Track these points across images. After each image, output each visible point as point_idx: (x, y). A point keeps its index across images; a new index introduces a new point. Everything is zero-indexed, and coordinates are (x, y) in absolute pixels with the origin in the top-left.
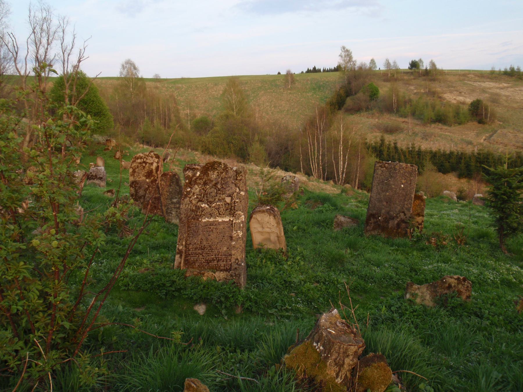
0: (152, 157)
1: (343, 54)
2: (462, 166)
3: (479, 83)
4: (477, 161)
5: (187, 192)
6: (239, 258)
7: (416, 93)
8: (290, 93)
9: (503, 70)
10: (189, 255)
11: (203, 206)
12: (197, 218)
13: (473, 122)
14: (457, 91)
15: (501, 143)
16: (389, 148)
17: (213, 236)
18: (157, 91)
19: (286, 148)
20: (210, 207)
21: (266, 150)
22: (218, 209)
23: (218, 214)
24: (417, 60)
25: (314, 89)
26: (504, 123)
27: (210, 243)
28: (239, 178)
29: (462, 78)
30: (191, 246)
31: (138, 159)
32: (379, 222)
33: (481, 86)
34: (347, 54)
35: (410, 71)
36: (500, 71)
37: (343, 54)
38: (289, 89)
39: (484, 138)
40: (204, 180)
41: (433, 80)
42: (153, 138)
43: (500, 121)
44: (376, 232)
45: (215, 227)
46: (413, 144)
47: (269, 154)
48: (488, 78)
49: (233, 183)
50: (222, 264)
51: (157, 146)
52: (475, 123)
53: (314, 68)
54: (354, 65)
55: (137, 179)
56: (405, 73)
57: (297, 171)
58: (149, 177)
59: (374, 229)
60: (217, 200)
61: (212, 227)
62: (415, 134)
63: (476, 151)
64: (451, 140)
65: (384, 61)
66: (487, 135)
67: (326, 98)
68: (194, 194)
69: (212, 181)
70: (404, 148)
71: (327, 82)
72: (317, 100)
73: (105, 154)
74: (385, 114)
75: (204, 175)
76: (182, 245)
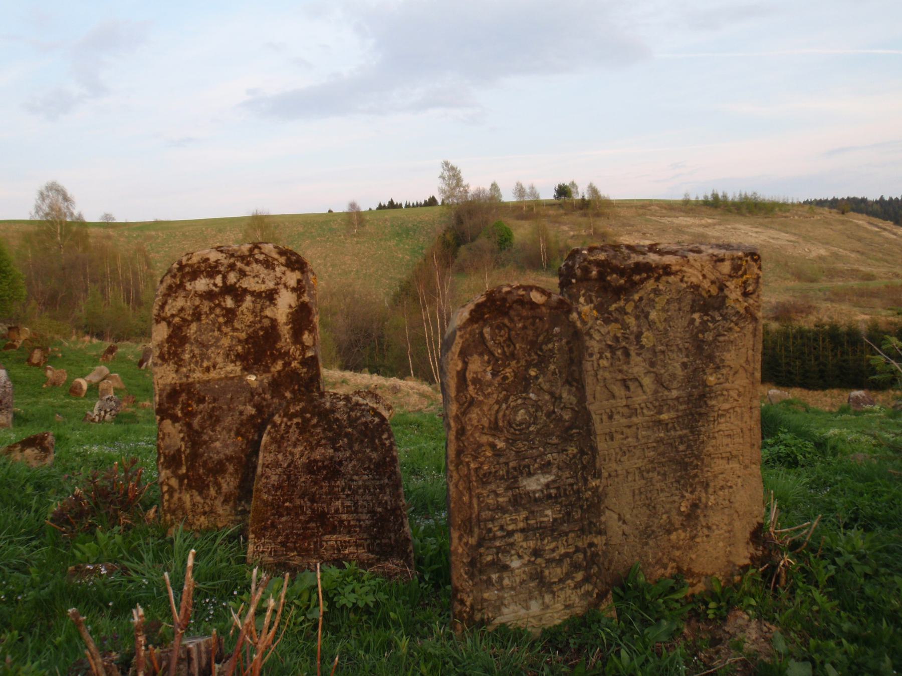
0: (268, 264)
1: (446, 174)
3: (669, 219)
7: (574, 236)
8: (357, 243)
9: (701, 198)
14: (638, 231)
18: (110, 243)
24: (567, 184)
25: (398, 235)
29: (641, 211)
31: (195, 274)
33: (672, 223)
34: (453, 175)
35: (557, 201)
36: (697, 201)
37: (446, 174)
38: (354, 236)
41: (598, 215)
42: (108, 325)
48: (681, 211)
51: (119, 339)
53: (391, 203)
54: (466, 192)
55: (197, 375)
56: (549, 205)
57: (406, 376)
58: (257, 361)
65: (513, 186)
67: (422, 248)
71: (420, 222)
72: (403, 257)
73: (7, 357)
74: (528, 272)
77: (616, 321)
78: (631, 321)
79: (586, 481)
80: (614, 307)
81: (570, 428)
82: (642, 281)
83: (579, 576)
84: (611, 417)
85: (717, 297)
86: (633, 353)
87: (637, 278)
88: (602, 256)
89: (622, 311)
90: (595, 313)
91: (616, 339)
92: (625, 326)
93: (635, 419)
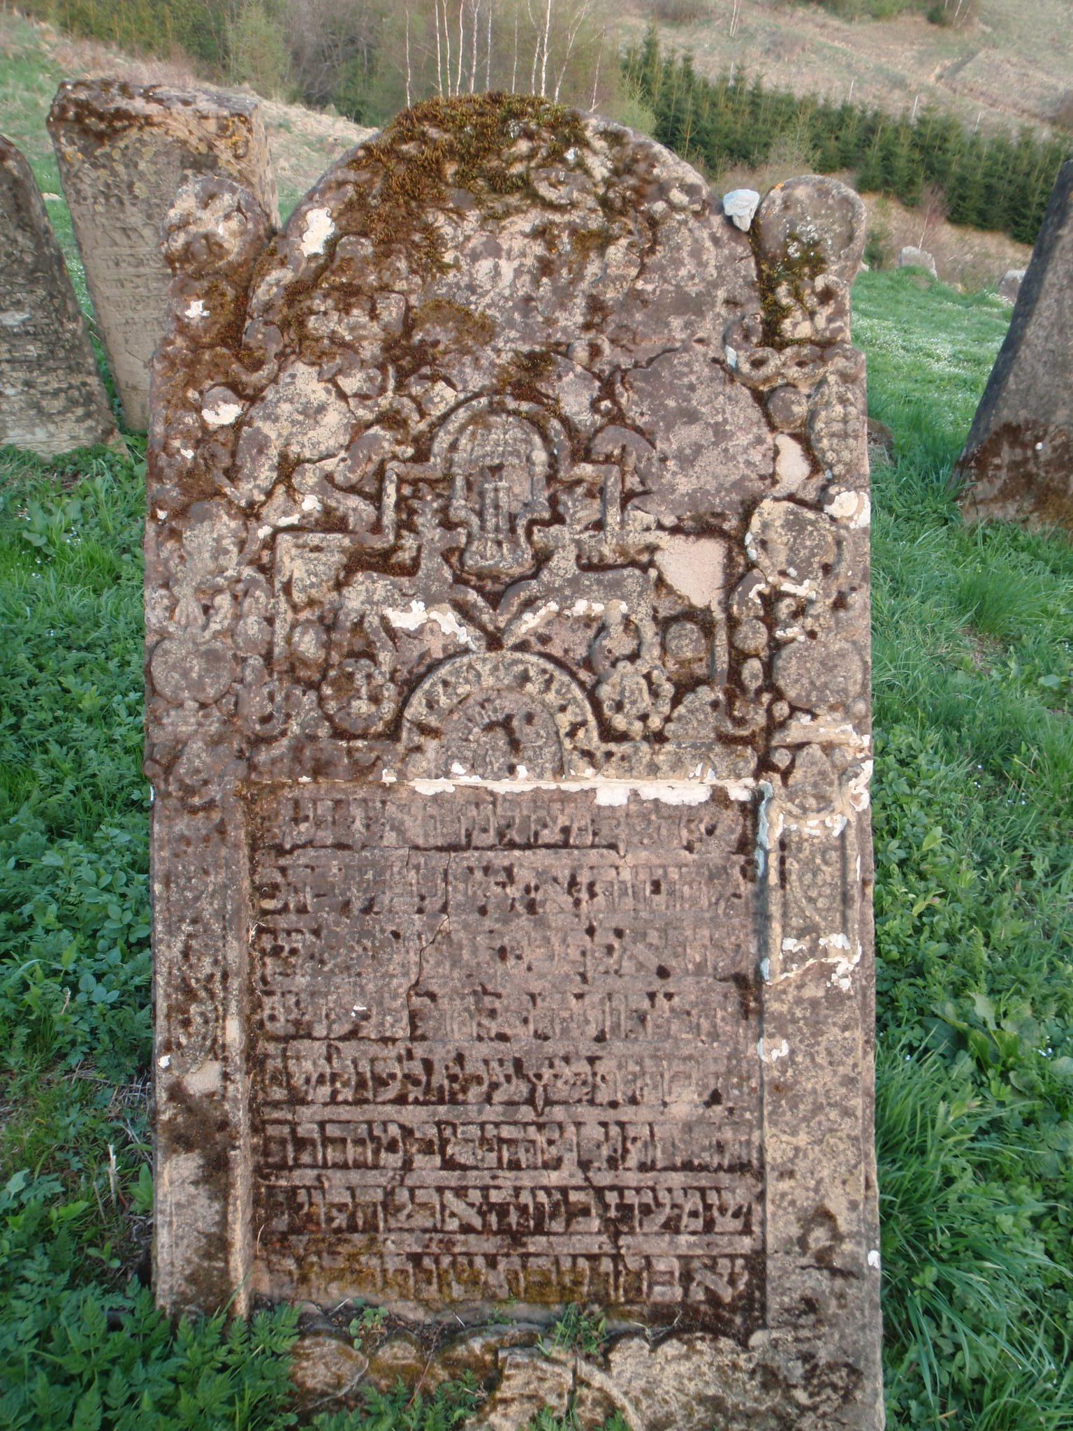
2: (874, 154)
4: (914, 145)
5: (203, 438)
6: (837, 1204)
10: (301, 1144)
11: (408, 618)
12: (359, 750)
13: (913, 14)
15: (982, 94)
16: (668, 75)
17: (545, 956)
19: (353, 41)
20: (494, 641)
21: (287, 41)
22: (588, 670)
23: (591, 738)
26: (995, 29)
27: (523, 1035)
28: (797, 327)
30: (308, 1062)
32: (1031, 467)
39: (938, 70)
40: (391, 311)
43: (986, 23)
44: (1011, 509)
45: (561, 865)
46: (741, 69)
47: (297, 56)
49: (732, 374)
50: (660, 1250)
52: (918, 19)
59: (1005, 494)
60: (564, 564)
61: (527, 865)
62: (746, 34)
63: (915, 112)
64: (849, 66)
66: (948, 63)
68: (288, 468)
69: (486, 330)
70: (713, 77)
75: (385, 250)
76: (217, 1050)
77: (104, 166)
78: (120, 168)
79: (62, 324)
80: (98, 152)
81: (34, 271)
82: (125, 128)
83: (80, 411)
84: (117, 264)
85: (208, 155)
86: (127, 203)
87: (118, 124)
88: (83, 95)
89: (108, 156)
90: (80, 155)
91: (108, 186)
92: (114, 173)
93: (142, 270)
